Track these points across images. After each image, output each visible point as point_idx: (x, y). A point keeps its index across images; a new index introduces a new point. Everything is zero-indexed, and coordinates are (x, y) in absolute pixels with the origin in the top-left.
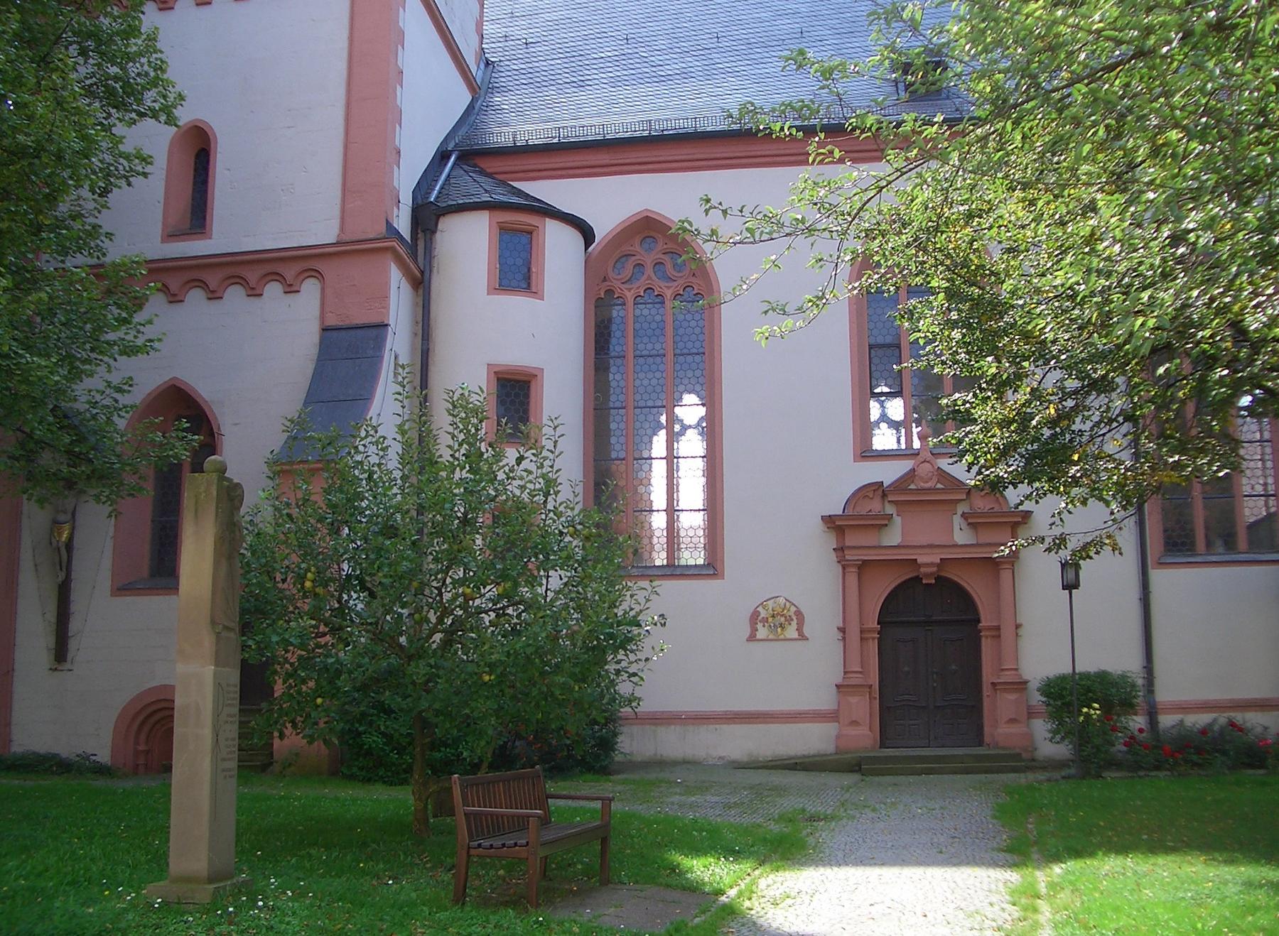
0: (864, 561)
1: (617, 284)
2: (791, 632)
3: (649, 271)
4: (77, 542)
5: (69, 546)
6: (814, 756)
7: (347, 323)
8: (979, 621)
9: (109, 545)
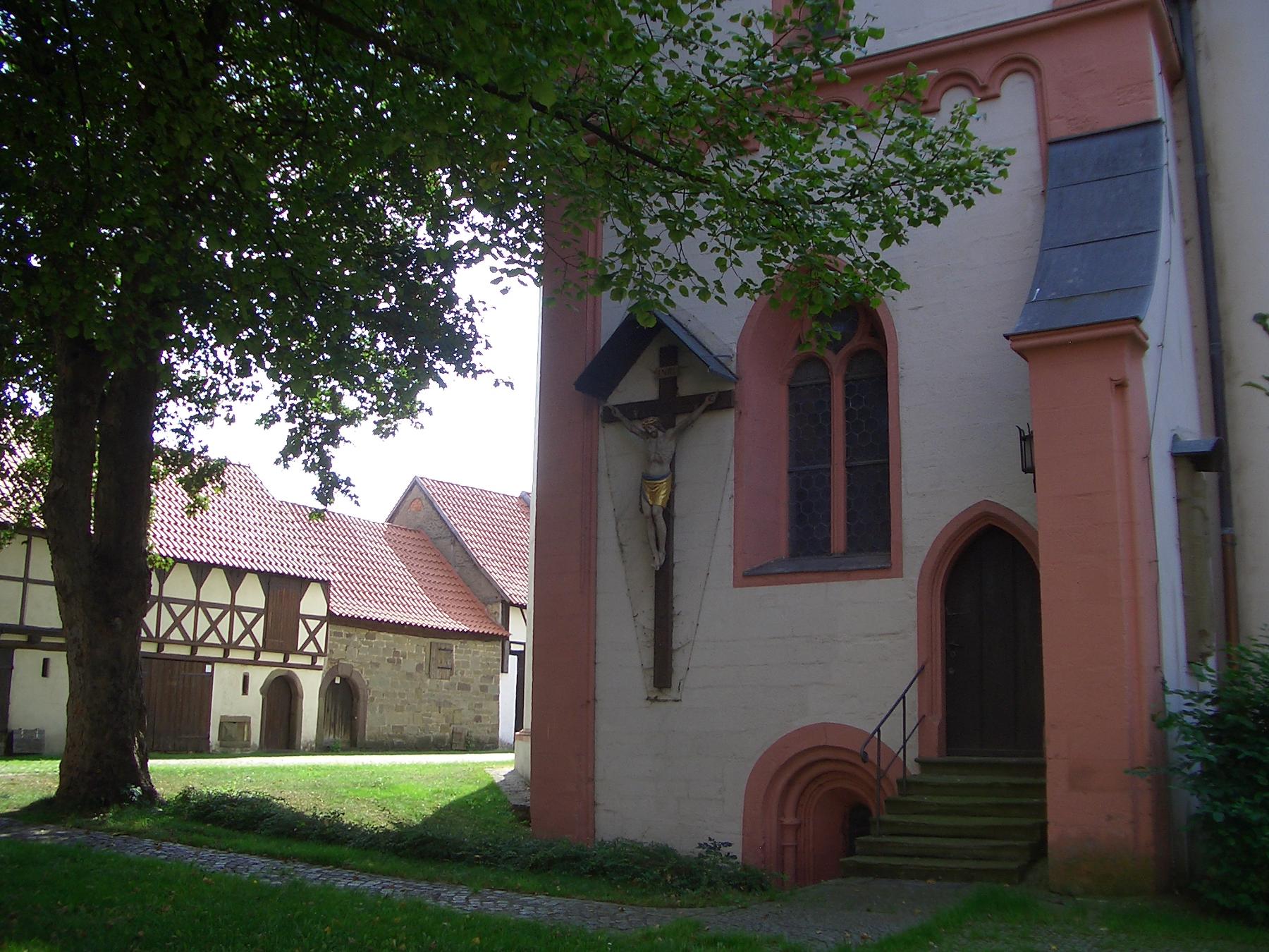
4: (678, 509)
5: (668, 512)
7: (1087, 130)
9: (728, 507)
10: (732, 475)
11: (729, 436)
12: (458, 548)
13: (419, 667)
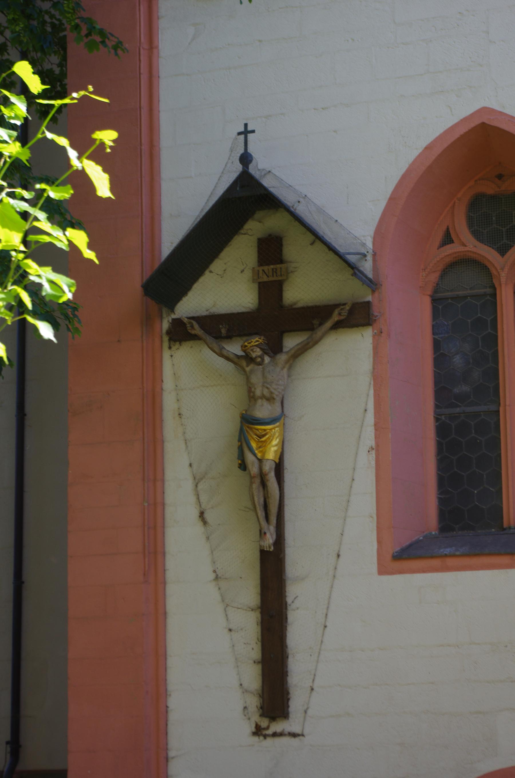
4: (287, 463)
10: (370, 418)
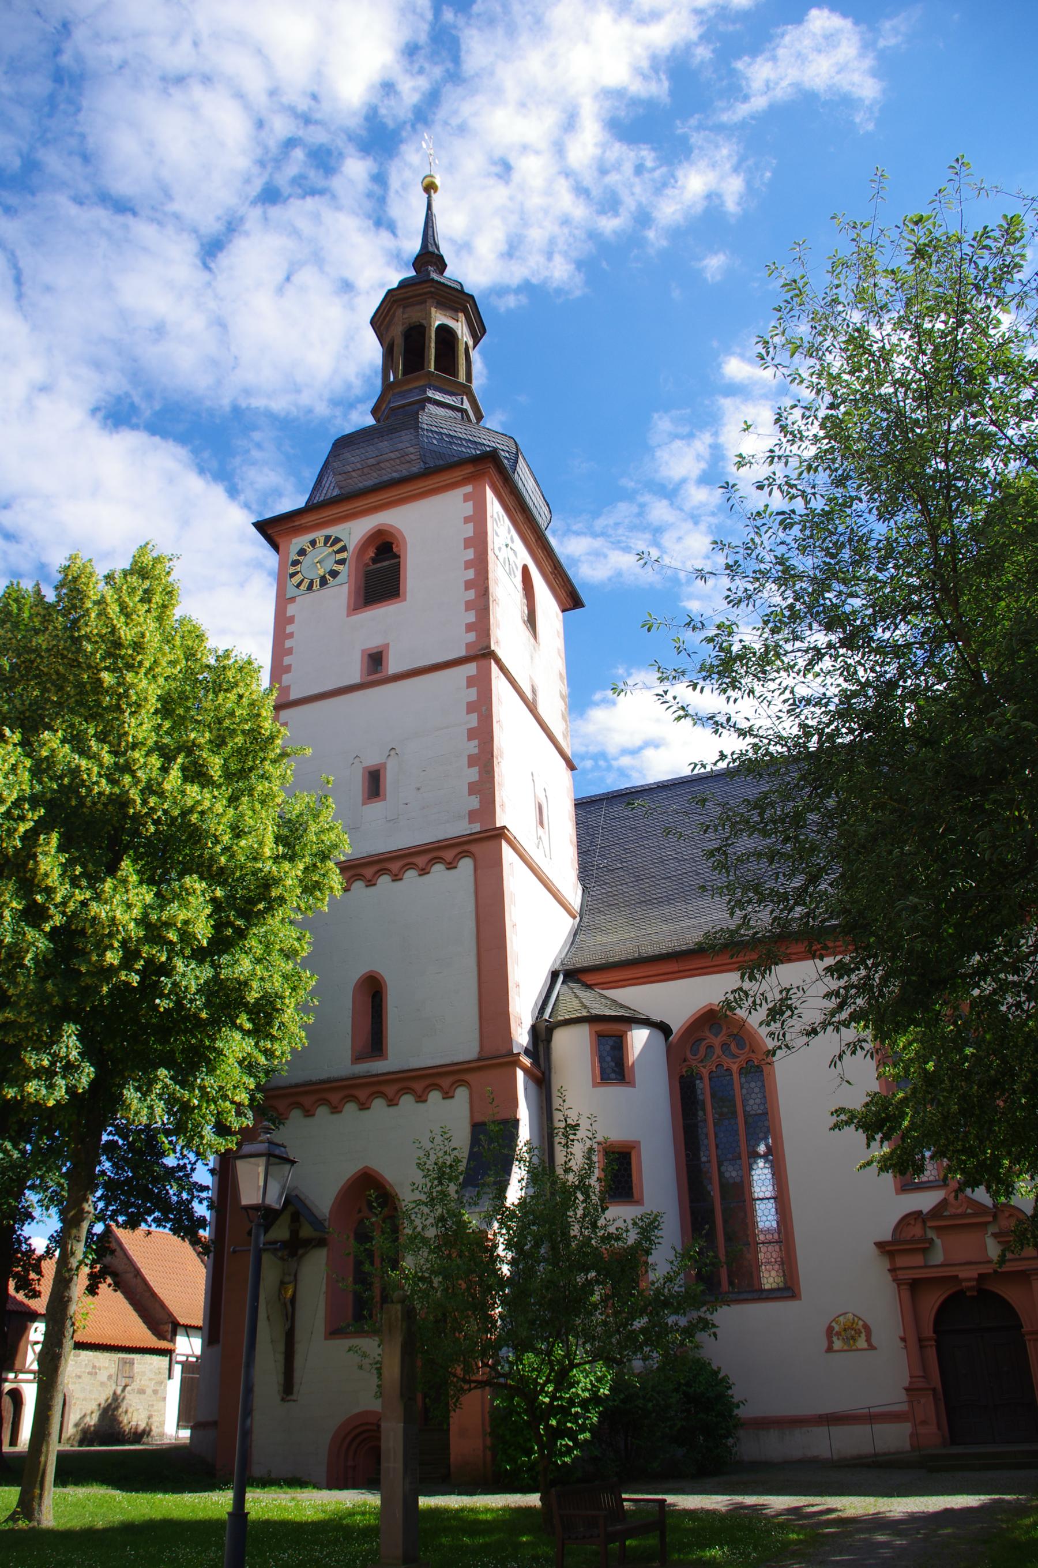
0: (914, 1279)
1: (694, 1063)
2: (862, 1343)
3: (718, 1051)
6: (894, 1454)
8: (1022, 1326)
11: (324, 1261)
12: (139, 1280)
13: (110, 1377)
